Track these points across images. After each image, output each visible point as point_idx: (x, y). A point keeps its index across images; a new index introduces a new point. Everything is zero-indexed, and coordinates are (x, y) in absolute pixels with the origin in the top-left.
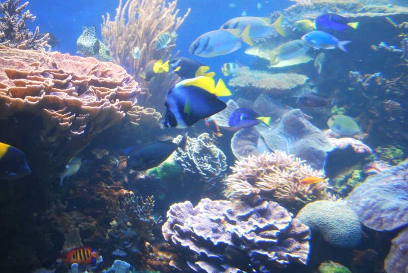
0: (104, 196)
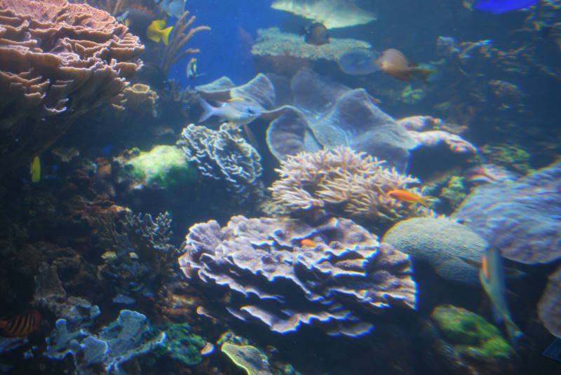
0: (87, 217)
